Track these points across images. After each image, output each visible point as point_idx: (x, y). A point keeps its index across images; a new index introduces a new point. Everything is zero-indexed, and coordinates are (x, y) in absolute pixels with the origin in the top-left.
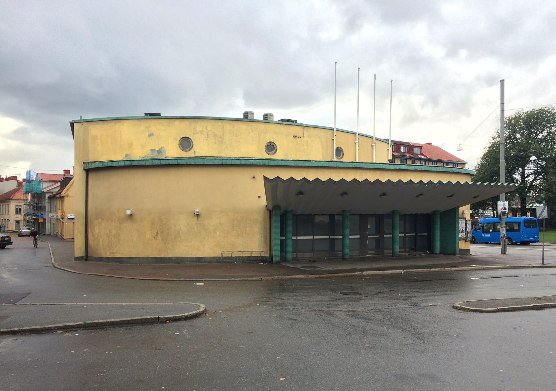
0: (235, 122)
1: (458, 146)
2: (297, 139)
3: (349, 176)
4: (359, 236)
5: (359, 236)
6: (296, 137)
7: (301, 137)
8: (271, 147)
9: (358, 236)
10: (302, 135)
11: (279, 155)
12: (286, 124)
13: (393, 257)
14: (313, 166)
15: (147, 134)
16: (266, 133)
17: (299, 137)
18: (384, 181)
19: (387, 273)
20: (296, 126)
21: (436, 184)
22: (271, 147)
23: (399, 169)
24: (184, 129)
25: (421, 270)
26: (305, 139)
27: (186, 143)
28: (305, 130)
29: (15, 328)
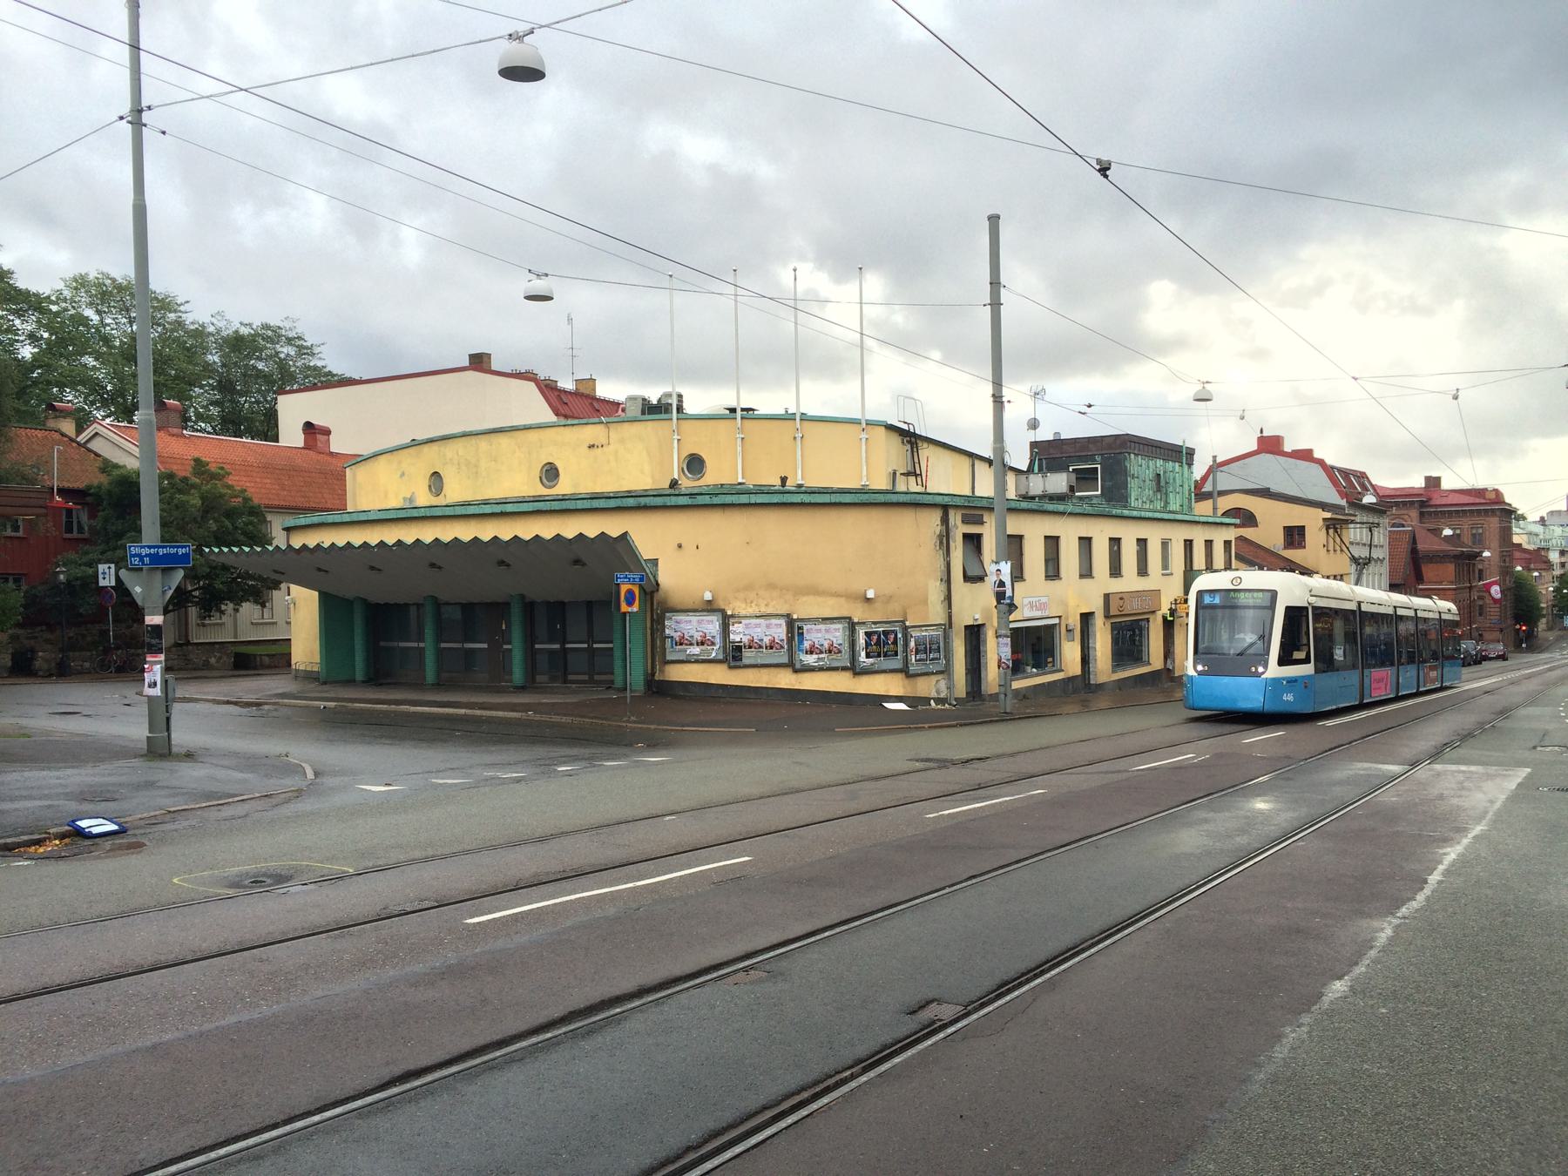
0: (492, 435)
1: (1200, 387)
2: (595, 450)
3: (570, 528)
4: (141, 590)
5: (141, 590)
6: (593, 446)
7: (602, 446)
8: (695, 464)
9: (485, 646)
10: (604, 441)
11: (564, 487)
12: (573, 425)
13: (419, 685)
14: (757, 502)
15: (399, 473)
16: (541, 447)
17: (600, 446)
18: (430, 541)
19: (526, 745)
20: (593, 426)
21: (393, 545)
22: (695, 464)
23: (502, 512)
24: (431, 458)
25: (362, 705)
26: (612, 447)
27: (436, 482)
28: (611, 429)
29: (655, 729)
